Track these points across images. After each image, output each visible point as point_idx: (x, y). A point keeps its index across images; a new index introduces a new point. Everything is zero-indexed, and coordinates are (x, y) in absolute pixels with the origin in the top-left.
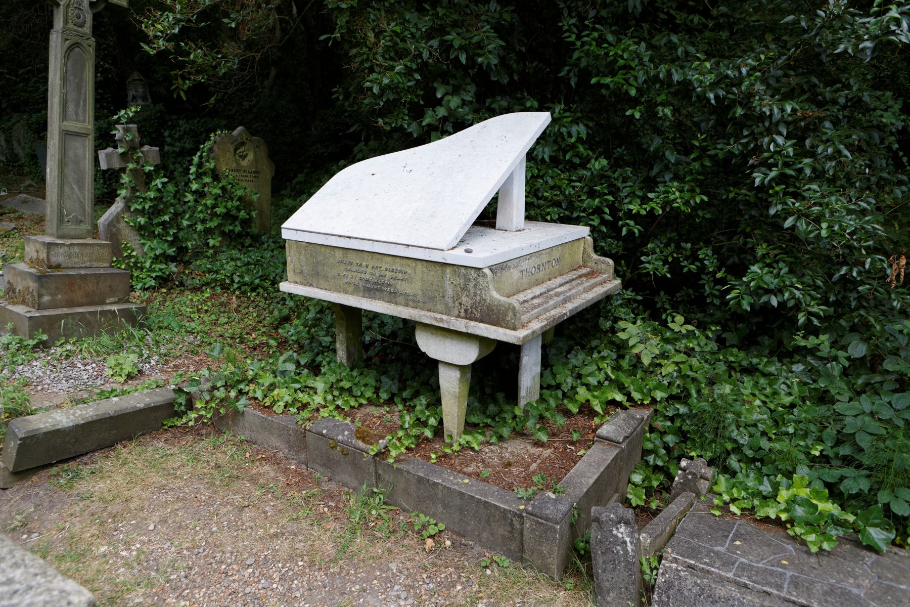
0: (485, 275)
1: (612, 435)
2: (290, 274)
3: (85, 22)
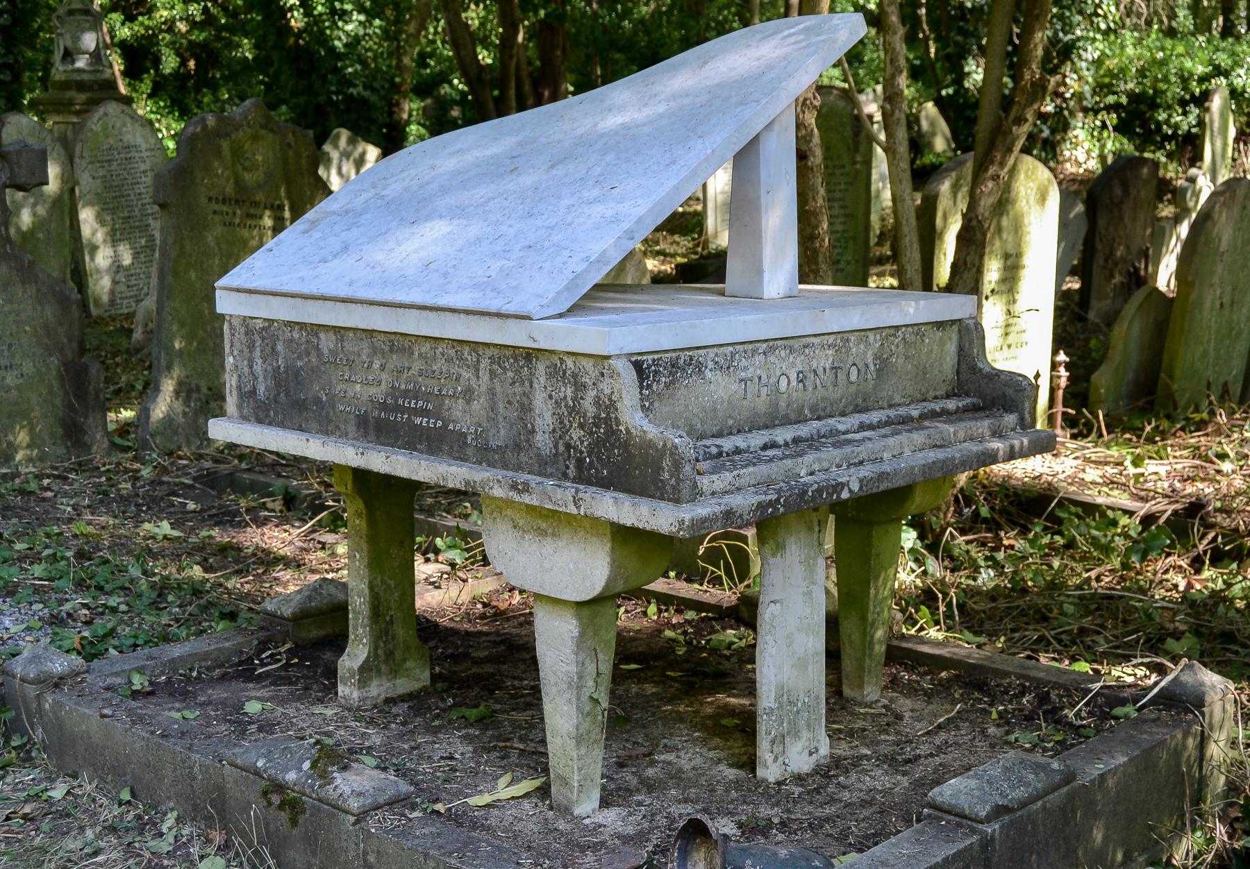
0: (614, 374)
1: (964, 803)
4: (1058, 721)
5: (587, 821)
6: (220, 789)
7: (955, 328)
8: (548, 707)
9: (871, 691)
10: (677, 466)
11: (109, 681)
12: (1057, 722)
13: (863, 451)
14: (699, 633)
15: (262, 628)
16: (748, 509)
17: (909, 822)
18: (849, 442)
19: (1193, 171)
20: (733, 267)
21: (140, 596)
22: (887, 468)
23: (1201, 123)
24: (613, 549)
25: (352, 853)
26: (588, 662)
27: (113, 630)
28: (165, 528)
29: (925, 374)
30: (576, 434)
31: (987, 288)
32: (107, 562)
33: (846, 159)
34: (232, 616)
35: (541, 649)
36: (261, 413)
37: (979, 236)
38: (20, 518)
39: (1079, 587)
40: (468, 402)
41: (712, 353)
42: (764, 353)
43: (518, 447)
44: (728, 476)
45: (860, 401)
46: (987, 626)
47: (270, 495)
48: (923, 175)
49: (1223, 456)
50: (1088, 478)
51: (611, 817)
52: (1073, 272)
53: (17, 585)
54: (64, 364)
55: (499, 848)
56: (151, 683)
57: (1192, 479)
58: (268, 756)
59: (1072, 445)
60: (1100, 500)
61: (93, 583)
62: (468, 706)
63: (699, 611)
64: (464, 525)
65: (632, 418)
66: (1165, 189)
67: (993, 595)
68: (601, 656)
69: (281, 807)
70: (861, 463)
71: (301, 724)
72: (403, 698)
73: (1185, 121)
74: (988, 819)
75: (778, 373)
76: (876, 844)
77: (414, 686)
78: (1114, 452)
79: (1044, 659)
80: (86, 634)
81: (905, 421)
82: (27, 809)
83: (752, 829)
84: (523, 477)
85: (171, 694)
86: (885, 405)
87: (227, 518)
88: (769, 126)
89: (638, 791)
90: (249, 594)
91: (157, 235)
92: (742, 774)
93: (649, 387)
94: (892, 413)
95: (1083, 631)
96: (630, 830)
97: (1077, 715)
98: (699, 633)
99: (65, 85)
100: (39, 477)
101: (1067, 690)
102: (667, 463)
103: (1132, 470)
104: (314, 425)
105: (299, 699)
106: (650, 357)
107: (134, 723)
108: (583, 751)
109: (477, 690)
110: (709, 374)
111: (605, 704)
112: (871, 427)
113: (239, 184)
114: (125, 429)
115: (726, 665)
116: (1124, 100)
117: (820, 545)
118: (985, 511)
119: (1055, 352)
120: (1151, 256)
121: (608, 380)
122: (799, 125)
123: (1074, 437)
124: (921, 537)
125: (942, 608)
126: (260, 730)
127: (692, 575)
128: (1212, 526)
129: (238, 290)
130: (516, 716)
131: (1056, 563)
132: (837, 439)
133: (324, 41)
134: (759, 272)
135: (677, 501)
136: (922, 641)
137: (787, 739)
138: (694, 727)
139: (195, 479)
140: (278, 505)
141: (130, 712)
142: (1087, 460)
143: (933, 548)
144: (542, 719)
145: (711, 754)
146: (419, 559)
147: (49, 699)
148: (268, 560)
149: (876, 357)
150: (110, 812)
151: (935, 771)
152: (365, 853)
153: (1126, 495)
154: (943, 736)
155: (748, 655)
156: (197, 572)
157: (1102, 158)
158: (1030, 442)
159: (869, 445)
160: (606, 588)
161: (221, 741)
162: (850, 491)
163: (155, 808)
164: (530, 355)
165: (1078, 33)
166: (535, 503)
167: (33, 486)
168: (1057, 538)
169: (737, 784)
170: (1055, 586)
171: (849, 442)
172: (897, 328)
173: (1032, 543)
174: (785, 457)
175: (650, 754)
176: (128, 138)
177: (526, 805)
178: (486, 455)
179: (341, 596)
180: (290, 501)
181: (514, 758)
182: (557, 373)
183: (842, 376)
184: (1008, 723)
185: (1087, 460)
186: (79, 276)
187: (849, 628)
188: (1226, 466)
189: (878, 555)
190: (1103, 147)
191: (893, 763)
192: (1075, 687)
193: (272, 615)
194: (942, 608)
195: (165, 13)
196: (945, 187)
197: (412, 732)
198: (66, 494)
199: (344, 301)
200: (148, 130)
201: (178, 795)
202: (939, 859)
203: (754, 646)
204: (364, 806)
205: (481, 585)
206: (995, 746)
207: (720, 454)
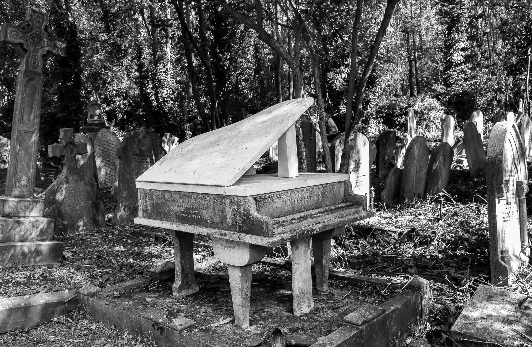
0: (249, 201)
1: (354, 320)
2: (140, 213)
3: (38, 66)
4: (378, 293)
5: (246, 330)
6: (140, 325)
8: (233, 297)
9: (325, 288)
10: (267, 226)
11: (107, 294)
12: (379, 295)
13: (319, 219)
14: (274, 273)
15: (150, 277)
17: (338, 327)
18: (315, 217)
19: (405, 134)
20: (280, 169)
21: (115, 268)
22: (326, 224)
23: (406, 120)
24: (250, 251)
25: (179, 342)
27: (108, 279)
28: (122, 248)
30: (238, 219)
31: (351, 170)
32: (106, 259)
33: (308, 136)
34: (141, 273)
35: (230, 280)
36: (149, 215)
37: (348, 156)
38: (81, 247)
39: (382, 254)
40: (208, 211)
43: (222, 223)
44: (282, 229)
46: (357, 267)
47: (151, 237)
48: (331, 138)
49: (420, 214)
50: (382, 222)
51: (253, 329)
52: (374, 164)
53: (81, 267)
54: (93, 203)
55: (221, 339)
56: (119, 294)
57: (412, 221)
58: (154, 314)
59: (377, 213)
60: (386, 229)
61: (102, 265)
62: (210, 297)
63: (274, 266)
64: (206, 244)
65: (255, 214)
66: (397, 139)
67: (358, 257)
69: (158, 329)
70: (319, 223)
71: (163, 304)
72: (191, 295)
73: (402, 120)
74: (362, 325)
76: (330, 333)
77: (194, 292)
78: (389, 215)
79: (373, 276)
80: (100, 280)
81: (331, 210)
82: (85, 332)
83: (294, 330)
84: (224, 231)
85: (125, 297)
87: (139, 244)
88: (288, 130)
89: (260, 320)
90: (146, 266)
91: (118, 165)
92: (289, 314)
93: (258, 204)
94: (327, 208)
95: (384, 267)
96: (258, 332)
97: (384, 292)
98: (274, 273)
99: (91, 124)
100: (86, 235)
101: (381, 285)
102: (264, 226)
103: (394, 220)
104: (164, 218)
105: (162, 297)
107: (115, 306)
109: (212, 292)
110: (275, 200)
111: (250, 296)
112: (321, 213)
113: (140, 150)
114: (110, 220)
115: (283, 282)
116: (384, 115)
117: (309, 247)
118: (354, 233)
119: (370, 187)
120: (395, 157)
121: (247, 203)
122: (296, 128)
123: (377, 211)
124: (336, 242)
125: (343, 262)
126: (151, 306)
127: (271, 255)
128: (418, 235)
129: (142, 181)
130: (223, 299)
131: (375, 248)
132: (312, 216)
133: (162, 108)
134: (287, 170)
135: (268, 237)
136: (338, 272)
138: (275, 300)
139: (130, 234)
140: (153, 240)
141: (114, 303)
142: (382, 217)
143: (340, 245)
144: (232, 300)
145: (280, 308)
146: (194, 254)
147: (91, 300)
148: (152, 256)
150: (108, 332)
151: (345, 310)
152: (182, 342)
153: (393, 227)
154: (346, 300)
155: (290, 278)
156: (131, 260)
157: (380, 131)
159: (321, 218)
160: (248, 262)
161: (140, 310)
163: (121, 330)
164: (224, 197)
165: (371, 97)
166: (228, 239)
167: (84, 238)
168: (375, 240)
169: (288, 317)
170: (376, 254)
171: (315, 217)
172: (327, 184)
173: (368, 242)
174: (298, 222)
175: (263, 309)
176: (109, 138)
177: (228, 326)
178: (213, 225)
179: (172, 266)
180: (157, 238)
181: (224, 312)
182: (232, 202)
183: (312, 198)
184: (365, 295)
185: (382, 217)
186: (96, 177)
187: (318, 270)
188: (421, 217)
190: (379, 128)
191: (333, 309)
192: (384, 284)
193: (153, 272)
194: (343, 262)
195: (118, 103)
196: (337, 142)
197: (194, 305)
198: (94, 240)
199: (172, 183)
200: (114, 136)
201: (128, 327)
202: (348, 337)
203: (291, 276)
205: (212, 261)
206: (362, 303)
207: (279, 222)
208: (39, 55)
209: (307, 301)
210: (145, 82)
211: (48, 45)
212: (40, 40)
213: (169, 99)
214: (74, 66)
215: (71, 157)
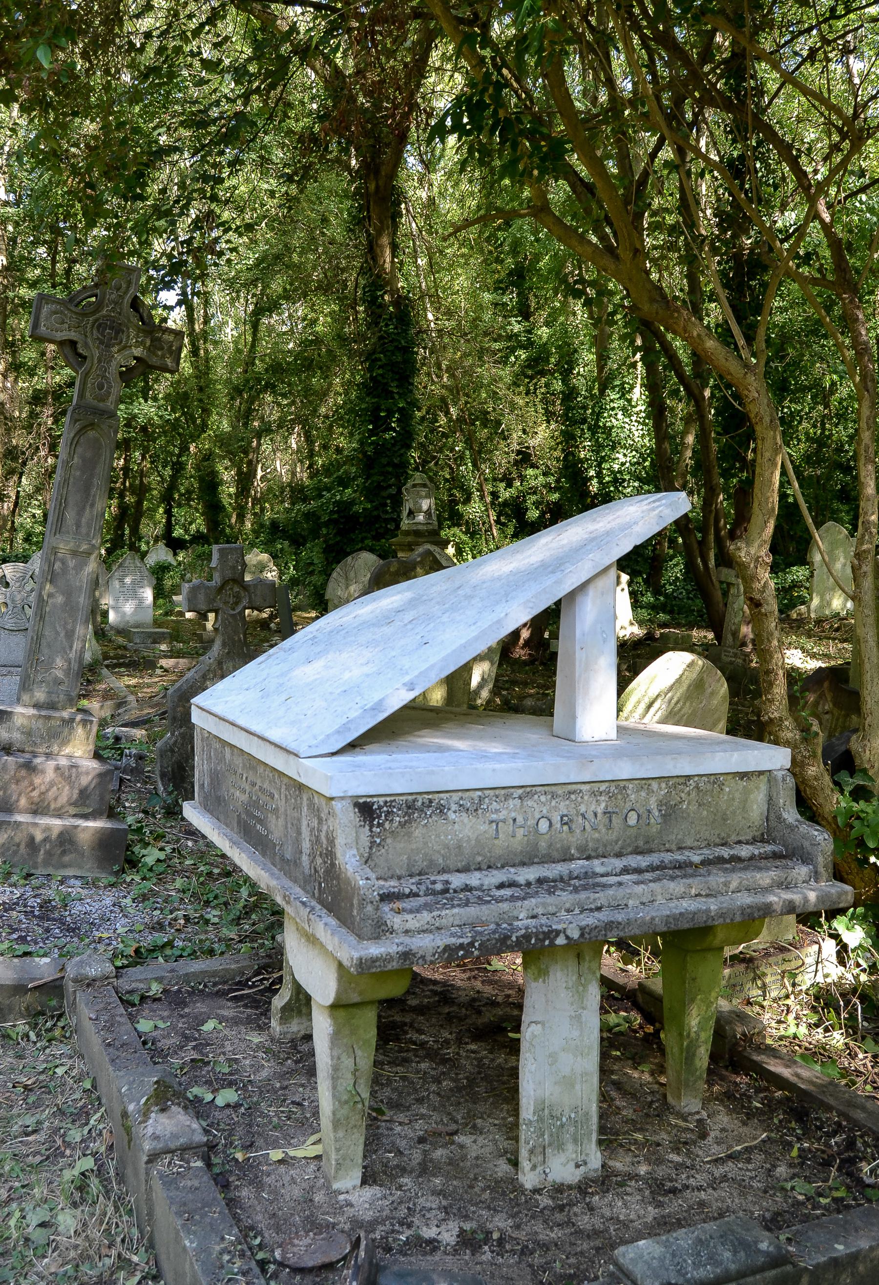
7: (763, 781)
12: (850, 1174)
16: (431, 951)
26: (344, 1057)
29: (725, 820)
41: (455, 797)
42: (520, 798)
45: (641, 843)
68: (359, 1053)
70: (599, 909)
75: (537, 816)
86: (674, 847)
106: (383, 799)
108: (341, 1134)
110: (452, 816)
137: (549, 1151)
149: (660, 804)
154: (729, 1167)
158: (818, 897)
162: (567, 937)
172: (689, 777)
183: (616, 821)
189: (694, 979)
204: (154, 1149)
207: (446, 891)
208: (113, 370)
209: (570, 1147)
210: (579, 433)
211: (138, 344)
212: (117, 333)
213: (627, 477)
214: (398, 393)
215: (233, 616)
